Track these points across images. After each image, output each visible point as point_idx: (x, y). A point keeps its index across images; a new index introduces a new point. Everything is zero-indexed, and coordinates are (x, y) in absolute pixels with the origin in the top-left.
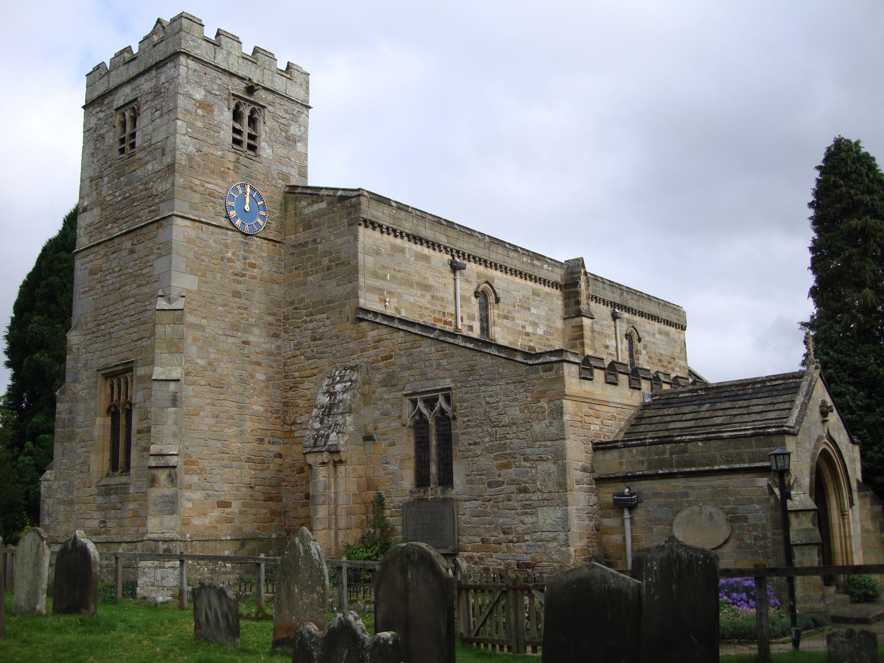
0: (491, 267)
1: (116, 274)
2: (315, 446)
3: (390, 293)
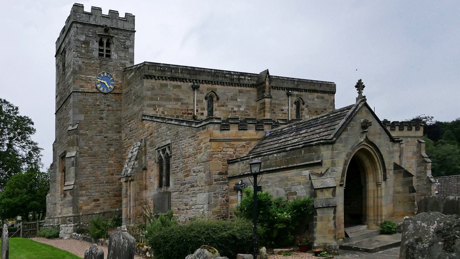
0: (215, 84)
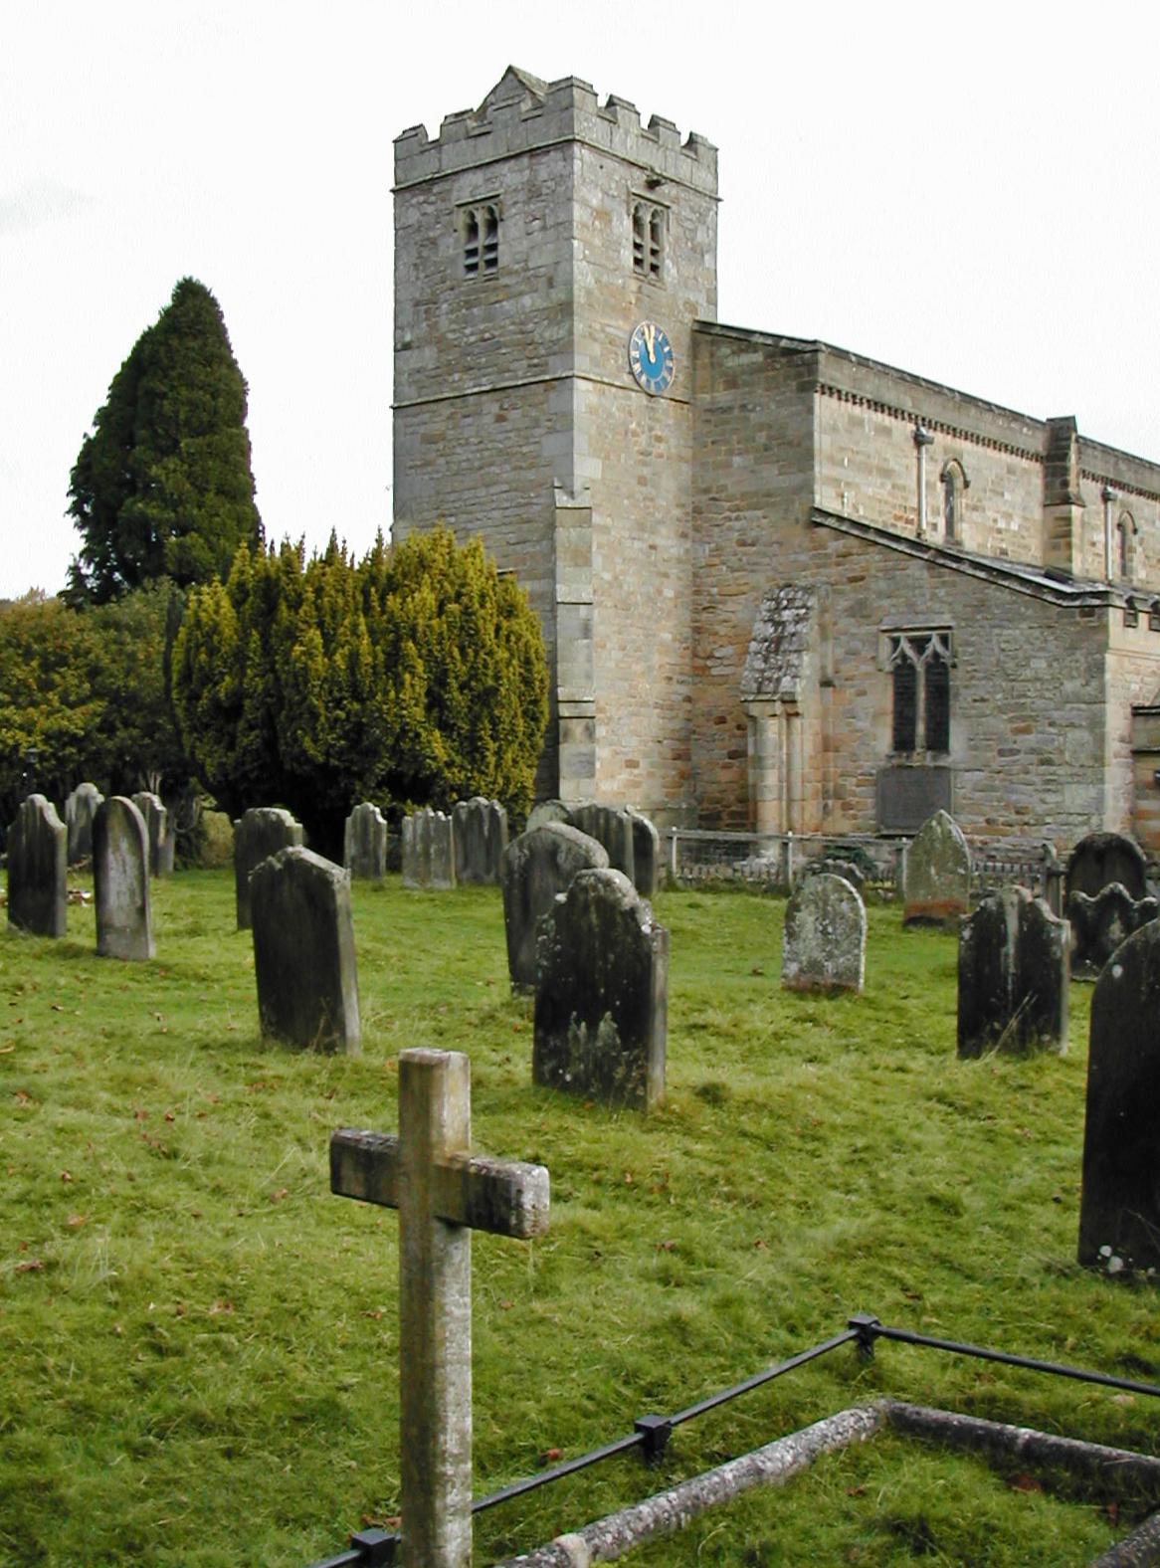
1: (474, 448)
2: (759, 692)
3: (848, 484)
